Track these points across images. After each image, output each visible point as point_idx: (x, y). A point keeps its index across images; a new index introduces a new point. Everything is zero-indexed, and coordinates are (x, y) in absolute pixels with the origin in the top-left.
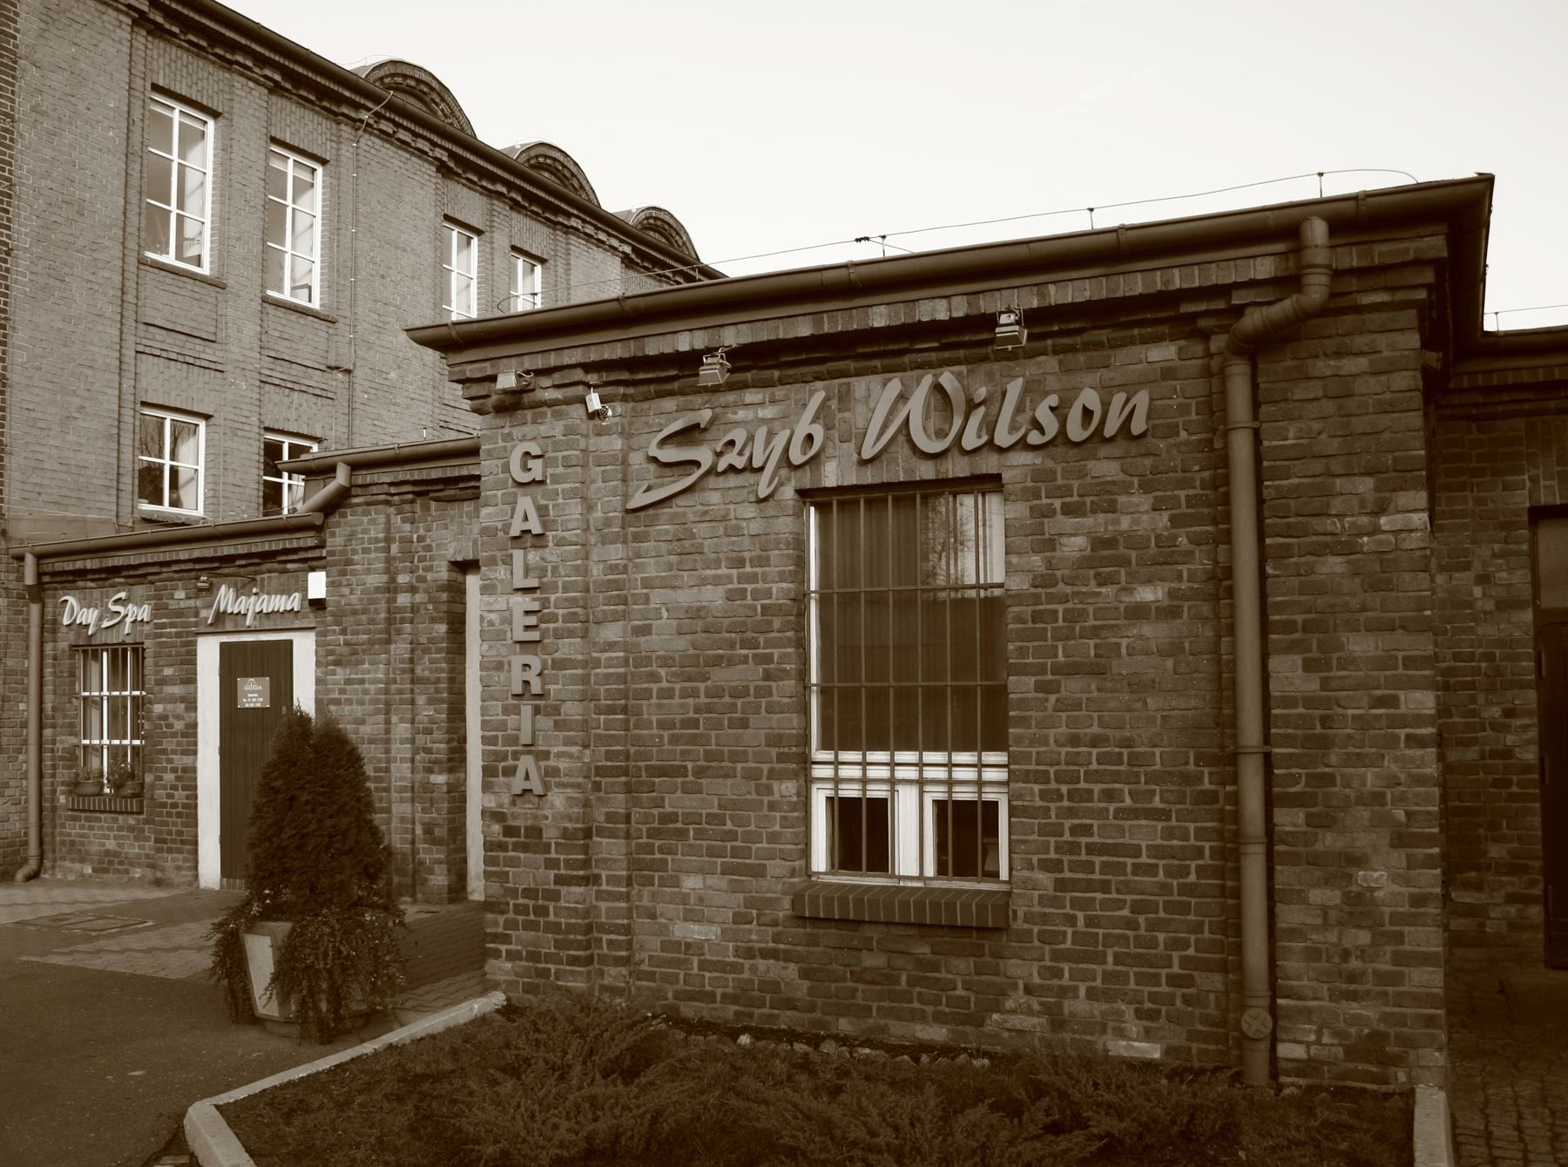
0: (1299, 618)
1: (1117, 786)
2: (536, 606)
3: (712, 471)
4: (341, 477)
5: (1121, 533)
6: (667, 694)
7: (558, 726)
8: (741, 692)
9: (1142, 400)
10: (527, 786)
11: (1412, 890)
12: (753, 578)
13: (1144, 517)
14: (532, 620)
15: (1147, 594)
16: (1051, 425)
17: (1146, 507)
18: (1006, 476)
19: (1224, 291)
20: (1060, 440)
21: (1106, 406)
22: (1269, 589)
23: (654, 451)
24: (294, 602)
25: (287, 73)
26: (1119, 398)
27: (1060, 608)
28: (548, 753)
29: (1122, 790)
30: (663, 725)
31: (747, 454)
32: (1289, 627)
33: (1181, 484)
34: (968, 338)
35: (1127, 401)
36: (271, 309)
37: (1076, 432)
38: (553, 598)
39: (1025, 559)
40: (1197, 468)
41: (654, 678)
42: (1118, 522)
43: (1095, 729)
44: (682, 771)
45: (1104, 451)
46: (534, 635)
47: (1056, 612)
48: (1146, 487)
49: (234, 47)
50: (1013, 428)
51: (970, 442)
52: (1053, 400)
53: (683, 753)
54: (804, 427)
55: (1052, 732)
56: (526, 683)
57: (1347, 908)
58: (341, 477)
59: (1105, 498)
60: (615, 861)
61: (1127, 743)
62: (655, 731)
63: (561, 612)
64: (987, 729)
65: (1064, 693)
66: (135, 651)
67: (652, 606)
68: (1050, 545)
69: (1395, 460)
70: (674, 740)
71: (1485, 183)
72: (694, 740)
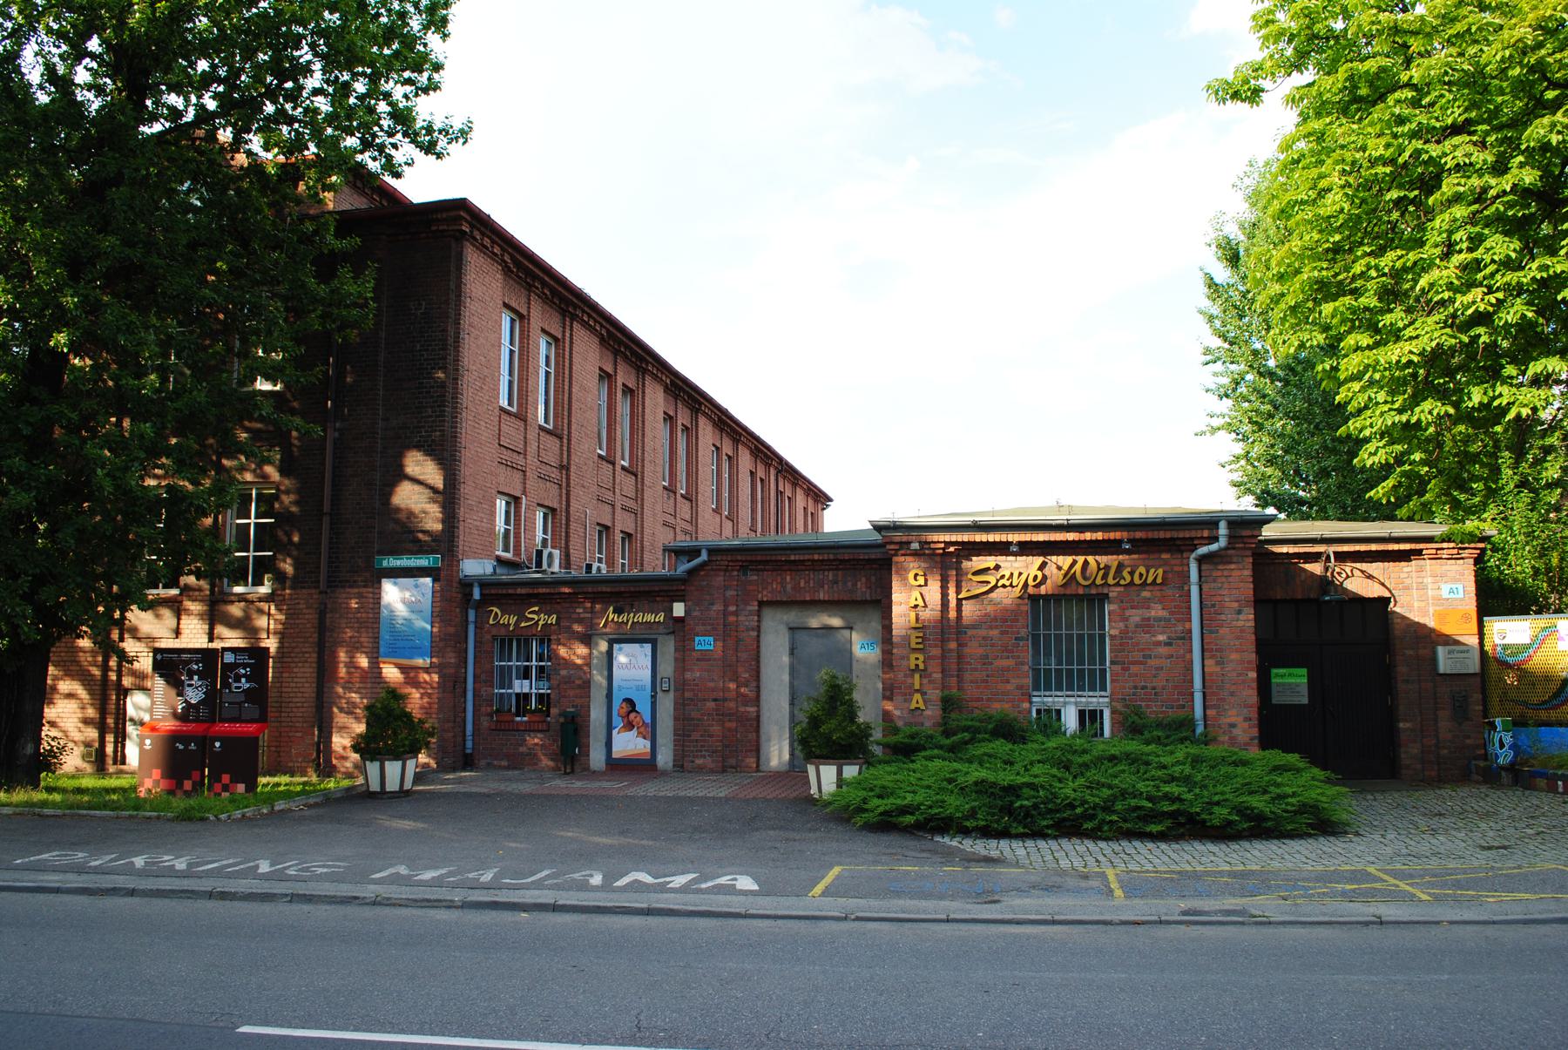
3: (996, 587)
4: (704, 556)
8: (1008, 669)
9: (1160, 571)
15: (1161, 638)
16: (1128, 579)
19: (1192, 539)
24: (661, 617)
25: (553, 290)
36: (504, 416)
37: (1137, 581)
49: (535, 277)
51: (1099, 581)
58: (704, 556)
64: (1095, 681)
66: (519, 641)
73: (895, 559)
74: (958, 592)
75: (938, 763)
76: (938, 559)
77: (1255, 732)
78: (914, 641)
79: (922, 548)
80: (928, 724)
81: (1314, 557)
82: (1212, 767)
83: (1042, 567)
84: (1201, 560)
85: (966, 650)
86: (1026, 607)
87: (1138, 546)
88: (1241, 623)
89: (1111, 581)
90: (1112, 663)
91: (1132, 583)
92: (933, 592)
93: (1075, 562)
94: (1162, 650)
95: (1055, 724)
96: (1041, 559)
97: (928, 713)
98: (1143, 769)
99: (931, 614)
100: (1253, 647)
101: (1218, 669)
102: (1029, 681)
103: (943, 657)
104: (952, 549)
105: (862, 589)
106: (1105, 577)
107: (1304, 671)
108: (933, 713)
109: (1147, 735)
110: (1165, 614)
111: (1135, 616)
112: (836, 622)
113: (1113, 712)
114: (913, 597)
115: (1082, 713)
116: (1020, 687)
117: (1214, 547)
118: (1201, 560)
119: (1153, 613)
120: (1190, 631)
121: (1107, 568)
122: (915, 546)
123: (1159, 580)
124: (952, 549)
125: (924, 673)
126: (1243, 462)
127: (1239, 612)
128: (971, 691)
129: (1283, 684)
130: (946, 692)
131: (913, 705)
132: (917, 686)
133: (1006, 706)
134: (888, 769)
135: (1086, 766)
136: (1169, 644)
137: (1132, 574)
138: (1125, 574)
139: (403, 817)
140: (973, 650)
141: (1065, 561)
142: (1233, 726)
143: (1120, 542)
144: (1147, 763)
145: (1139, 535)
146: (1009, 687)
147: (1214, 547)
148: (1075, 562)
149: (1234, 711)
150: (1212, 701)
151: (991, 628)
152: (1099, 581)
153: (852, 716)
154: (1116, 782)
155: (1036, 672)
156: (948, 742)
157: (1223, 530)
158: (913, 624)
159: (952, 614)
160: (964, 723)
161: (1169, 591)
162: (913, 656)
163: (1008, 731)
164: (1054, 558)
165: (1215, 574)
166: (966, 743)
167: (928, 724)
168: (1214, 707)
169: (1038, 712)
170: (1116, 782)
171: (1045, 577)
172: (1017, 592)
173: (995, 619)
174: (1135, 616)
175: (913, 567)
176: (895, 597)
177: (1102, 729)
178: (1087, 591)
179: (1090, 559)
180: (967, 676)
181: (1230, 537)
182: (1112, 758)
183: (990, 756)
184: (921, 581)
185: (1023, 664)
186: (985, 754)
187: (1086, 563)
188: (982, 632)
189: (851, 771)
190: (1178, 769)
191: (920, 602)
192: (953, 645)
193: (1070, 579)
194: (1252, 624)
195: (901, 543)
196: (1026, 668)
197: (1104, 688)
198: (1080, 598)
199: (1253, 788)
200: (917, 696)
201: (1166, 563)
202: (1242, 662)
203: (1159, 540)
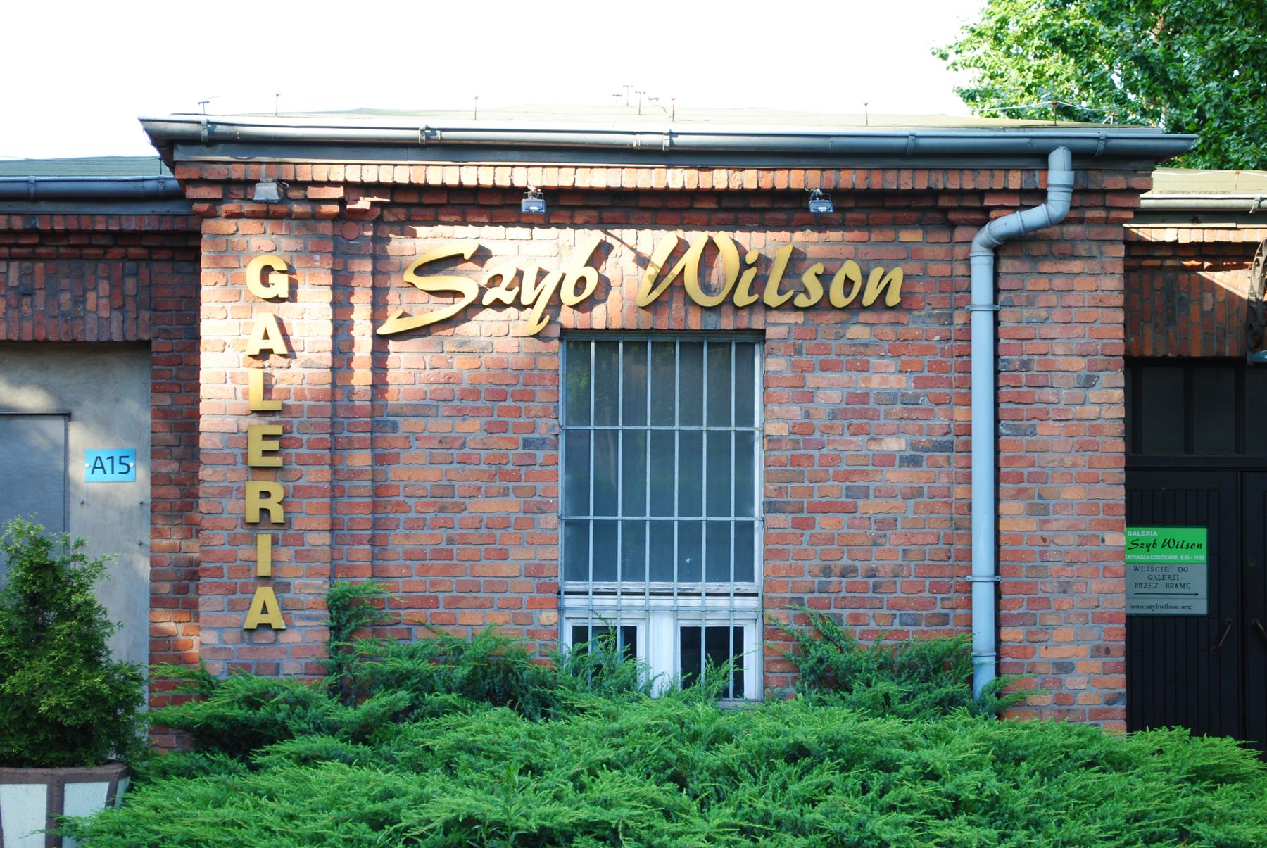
0: (1026, 471)
1: (861, 611)
2: (278, 430)
3: (476, 306)
5: (871, 390)
6: (420, 524)
7: (299, 556)
8: (504, 524)
9: (897, 275)
10: (265, 619)
11: (1105, 691)
12: (517, 412)
13: (893, 377)
14: (274, 445)
15: (894, 445)
17: (892, 369)
18: (771, 333)
19: (980, 194)
20: (823, 304)
21: (865, 277)
22: (1001, 446)
26: (876, 273)
27: (816, 453)
28: (288, 584)
29: (867, 615)
31: (516, 290)
32: (1019, 478)
33: (924, 351)
34: (779, 208)
35: (884, 276)
37: (838, 298)
38: (296, 422)
39: (785, 407)
40: (937, 338)
42: (866, 380)
43: (846, 561)
44: (435, 603)
45: (864, 317)
46: (276, 461)
47: (812, 457)
48: (895, 353)
50: (781, 292)
51: (742, 298)
52: (819, 268)
53: (433, 584)
55: (806, 565)
56: (264, 512)
57: (1056, 707)
59: (858, 359)
61: (872, 573)
63: (305, 437)
64: (727, 553)
65: (817, 530)
68: (809, 397)
69: (1104, 345)
70: (424, 571)
72: (445, 571)
73: (209, 226)
74: (377, 317)
75: (333, 772)
76: (326, 228)
77: (1117, 684)
78: (257, 446)
79: (285, 199)
80: (291, 667)
81: (1240, 255)
82: (1048, 774)
83: (599, 255)
84: (1002, 248)
85: (394, 473)
86: (554, 357)
87: (855, 208)
88: (1091, 411)
89: (772, 298)
90: (769, 507)
91: (825, 304)
92: (311, 315)
93: (680, 250)
94: (896, 477)
95: (624, 666)
96: (596, 236)
97: (293, 637)
98: (878, 780)
99: (305, 374)
100: (1119, 474)
101: (1031, 525)
102: (556, 554)
103: (335, 492)
104: (364, 203)
105: (99, 308)
106: (758, 285)
107: (1199, 535)
108: (306, 638)
109: (859, 692)
110: (903, 384)
111: (831, 390)
112: (30, 399)
113: (769, 634)
114: (257, 327)
115: (689, 638)
116: (534, 571)
117: (1035, 216)
118: (1002, 248)
119: (875, 382)
120: (967, 430)
121: (764, 262)
122: (267, 191)
123: (893, 299)
124: (364, 203)
125: (283, 532)
126: (986, 45)
127: (1089, 383)
128: (404, 580)
129: (1151, 567)
130: (342, 584)
131: (253, 618)
132: (264, 568)
133: (500, 617)
134: (196, 788)
135: (730, 773)
136: (913, 461)
137: (825, 278)
138: (809, 279)
139: (19, 383)
140: (414, 472)
141: (657, 242)
142: (1065, 667)
143: (799, 197)
144: (886, 766)
145: (850, 178)
146: (507, 568)
147: (1035, 216)
148: (680, 250)
149: (1066, 632)
150: (1016, 605)
151: (461, 413)
152: (742, 298)
153: (90, 650)
154: (816, 814)
155: (576, 530)
156: (350, 714)
157: (1059, 172)
158: (257, 402)
159: (361, 377)
160: (391, 664)
161: (919, 326)
162: (254, 488)
163: (496, 681)
164: (629, 235)
165: (1033, 283)
166: (397, 717)
167: (291, 667)
168: (1020, 620)
169: (580, 634)
170: (816, 814)
171: (604, 285)
172: (531, 321)
173: (474, 393)
174: (831, 390)
175: (262, 245)
176: (209, 328)
177: (739, 678)
178: (712, 322)
179: (723, 239)
180: (398, 541)
181: (1078, 192)
182: (796, 753)
183: (473, 750)
184: (280, 285)
185: (542, 508)
186: (461, 747)
187: (711, 248)
188: (439, 426)
189: (87, 799)
190: (969, 779)
191: (277, 344)
192: (361, 459)
193: (669, 289)
194: (1119, 412)
195: (227, 183)
196: (551, 519)
197: (745, 573)
198: (692, 342)
199: (1156, 826)
200: (265, 594)
201: (912, 254)
202: (1089, 508)
203: (898, 194)
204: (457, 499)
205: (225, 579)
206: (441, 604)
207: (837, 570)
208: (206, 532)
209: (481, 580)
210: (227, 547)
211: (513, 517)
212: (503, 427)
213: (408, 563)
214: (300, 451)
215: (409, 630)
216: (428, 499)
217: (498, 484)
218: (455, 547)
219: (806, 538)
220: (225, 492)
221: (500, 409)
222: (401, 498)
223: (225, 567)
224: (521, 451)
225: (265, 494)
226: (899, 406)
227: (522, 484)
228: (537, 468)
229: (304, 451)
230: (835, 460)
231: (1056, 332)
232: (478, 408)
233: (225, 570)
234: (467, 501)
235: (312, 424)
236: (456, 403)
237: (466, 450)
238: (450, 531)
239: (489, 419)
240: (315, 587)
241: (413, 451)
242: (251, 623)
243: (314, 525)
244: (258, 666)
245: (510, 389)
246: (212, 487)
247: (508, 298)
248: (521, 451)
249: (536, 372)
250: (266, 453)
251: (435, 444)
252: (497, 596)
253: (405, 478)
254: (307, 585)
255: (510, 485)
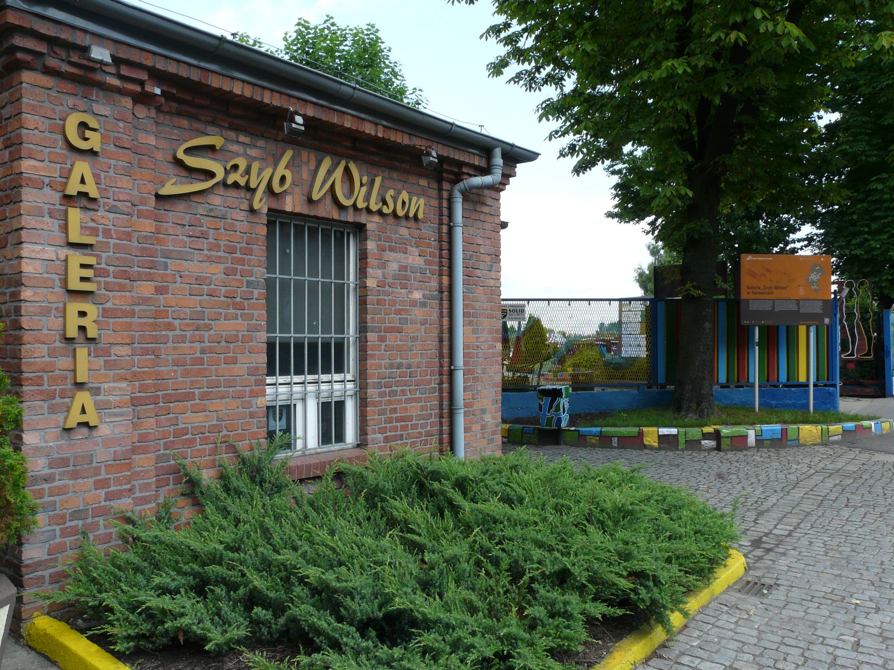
12: (242, 262)
14: (89, 273)
18: (369, 226)
19: (460, 164)
21: (410, 200)
23: (180, 155)
26: (414, 199)
27: (387, 298)
28: (99, 389)
30: (176, 363)
37: (400, 213)
41: (170, 327)
42: (407, 259)
43: (399, 360)
46: (86, 287)
54: (281, 170)
60: (146, 472)
62: (171, 367)
67: (169, 272)
70: (186, 374)
71: (537, 155)
72: (200, 373)
162: (74, 307)
204: (206, 321)
205: (45, 387)
206: (197, 398)
207: (395, 365)
208: (28, 346)
209: (222, 378)
210: (47, 359)
211: (240, 334)
212: (234, 272)
213: (175, 368)
214: (107, 279)
215: (177, 418)
216: (188, 321)
217: (232, 311)
218: (205, 356)
219: (383, 347)
220: (45, 312)
221: (232, 259)
222: (170, 320)
223: (45, 376)
224: (244, 289)
225: (83, 314)
226: (419, 274)
227: (246, 311)
228: (254, 301)
229: (110, 279)
230: (393, 303)
231: (480, 241)
232: (220, 257)
233: (46, 378)
234: (213, 323)
235: (117, 259)
236: (206, 252)
237: (212, 286)
238: (202, 344)
239: (226, 265)
240: (121, 389)
241: (178, 285)
242: (72, 423)
243: (119, 340)
244: (76, 458)
245: (238, 246)
246: (34, 307)
247: (242, 182)
248: (244, 289)
249: (254, 235)
250: (83, 279)
251: (193, 281)
252: (231, 389)
253: (173, 304)
254: (114, 387)
255: (239, 312)
